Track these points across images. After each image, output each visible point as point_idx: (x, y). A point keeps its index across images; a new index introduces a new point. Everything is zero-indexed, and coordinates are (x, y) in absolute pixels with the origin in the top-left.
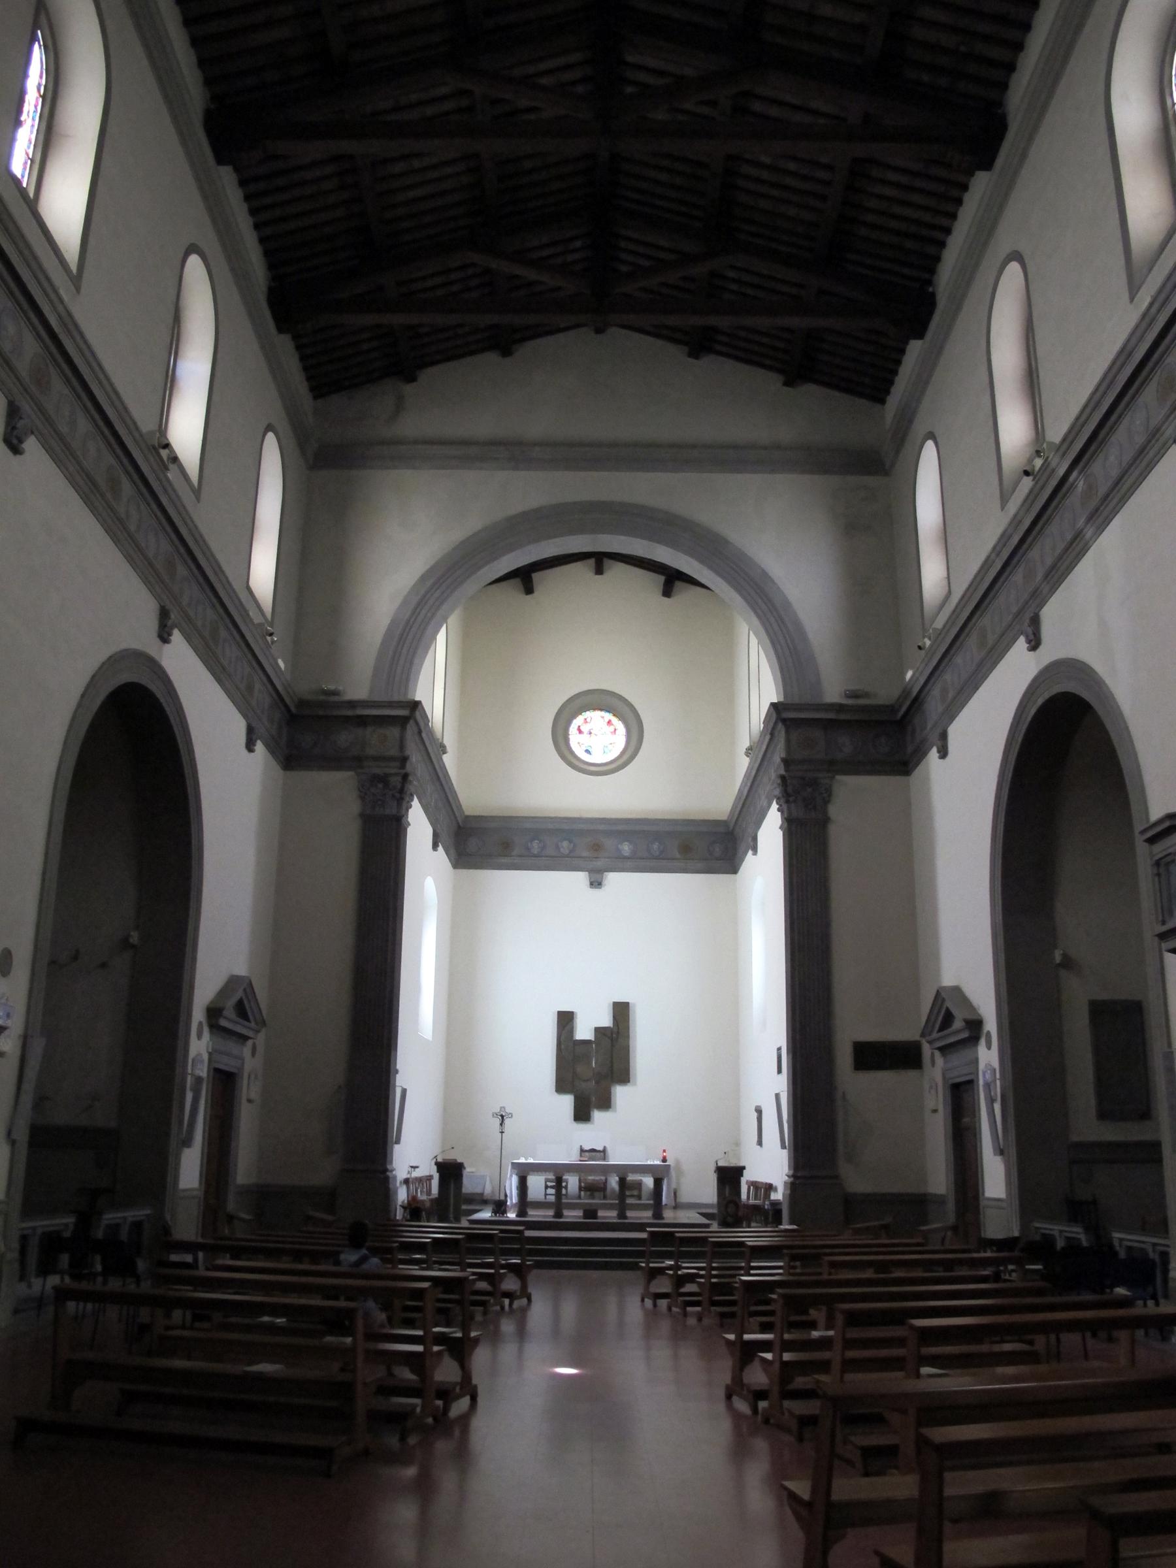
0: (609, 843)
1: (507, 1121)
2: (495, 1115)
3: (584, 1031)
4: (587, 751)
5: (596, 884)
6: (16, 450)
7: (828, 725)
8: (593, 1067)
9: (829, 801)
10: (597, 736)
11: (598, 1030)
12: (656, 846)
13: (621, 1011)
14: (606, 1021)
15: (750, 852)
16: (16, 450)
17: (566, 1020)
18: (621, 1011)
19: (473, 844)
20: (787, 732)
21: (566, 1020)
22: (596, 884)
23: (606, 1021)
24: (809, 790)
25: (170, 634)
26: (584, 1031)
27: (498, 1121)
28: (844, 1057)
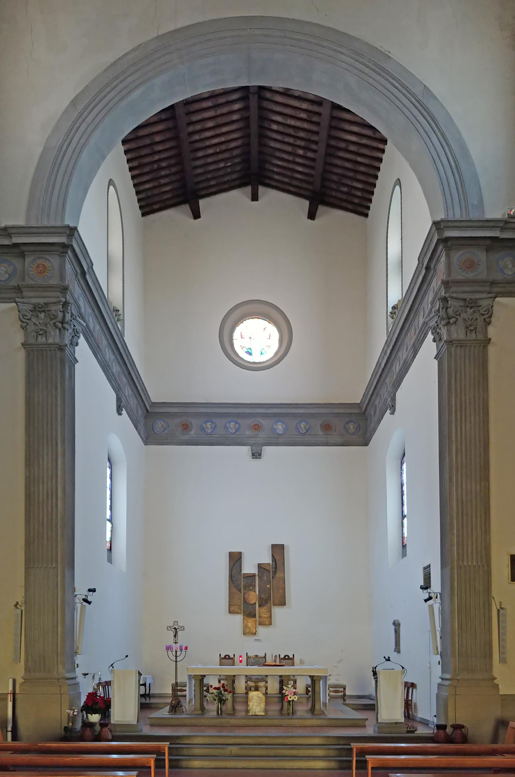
0: (265, 423)
1: (179, 633)
2: (169, 628)
3: (249, 567)
4: (250, 354)
5: (256, 455)
6: (120, 414)
7: (493, 244)
8: (257, 589)
9: (489, 323)
10: (257, 339)
11: (260, 566)
12: (303, 425)
13: (278, 550)
14: (267, 559)
15: (388, 411)
16: (120, 414)
17: (235, 559)
18: (278, 550)
19: (159, 425)
20: (448, 256)
21: (235, 559)
22: (256, 455)
23: (267, 559)
24: (470, 311)
25: (496, 684)
26: (249, 567)
27: (172, 634)
28: (501, 569)
